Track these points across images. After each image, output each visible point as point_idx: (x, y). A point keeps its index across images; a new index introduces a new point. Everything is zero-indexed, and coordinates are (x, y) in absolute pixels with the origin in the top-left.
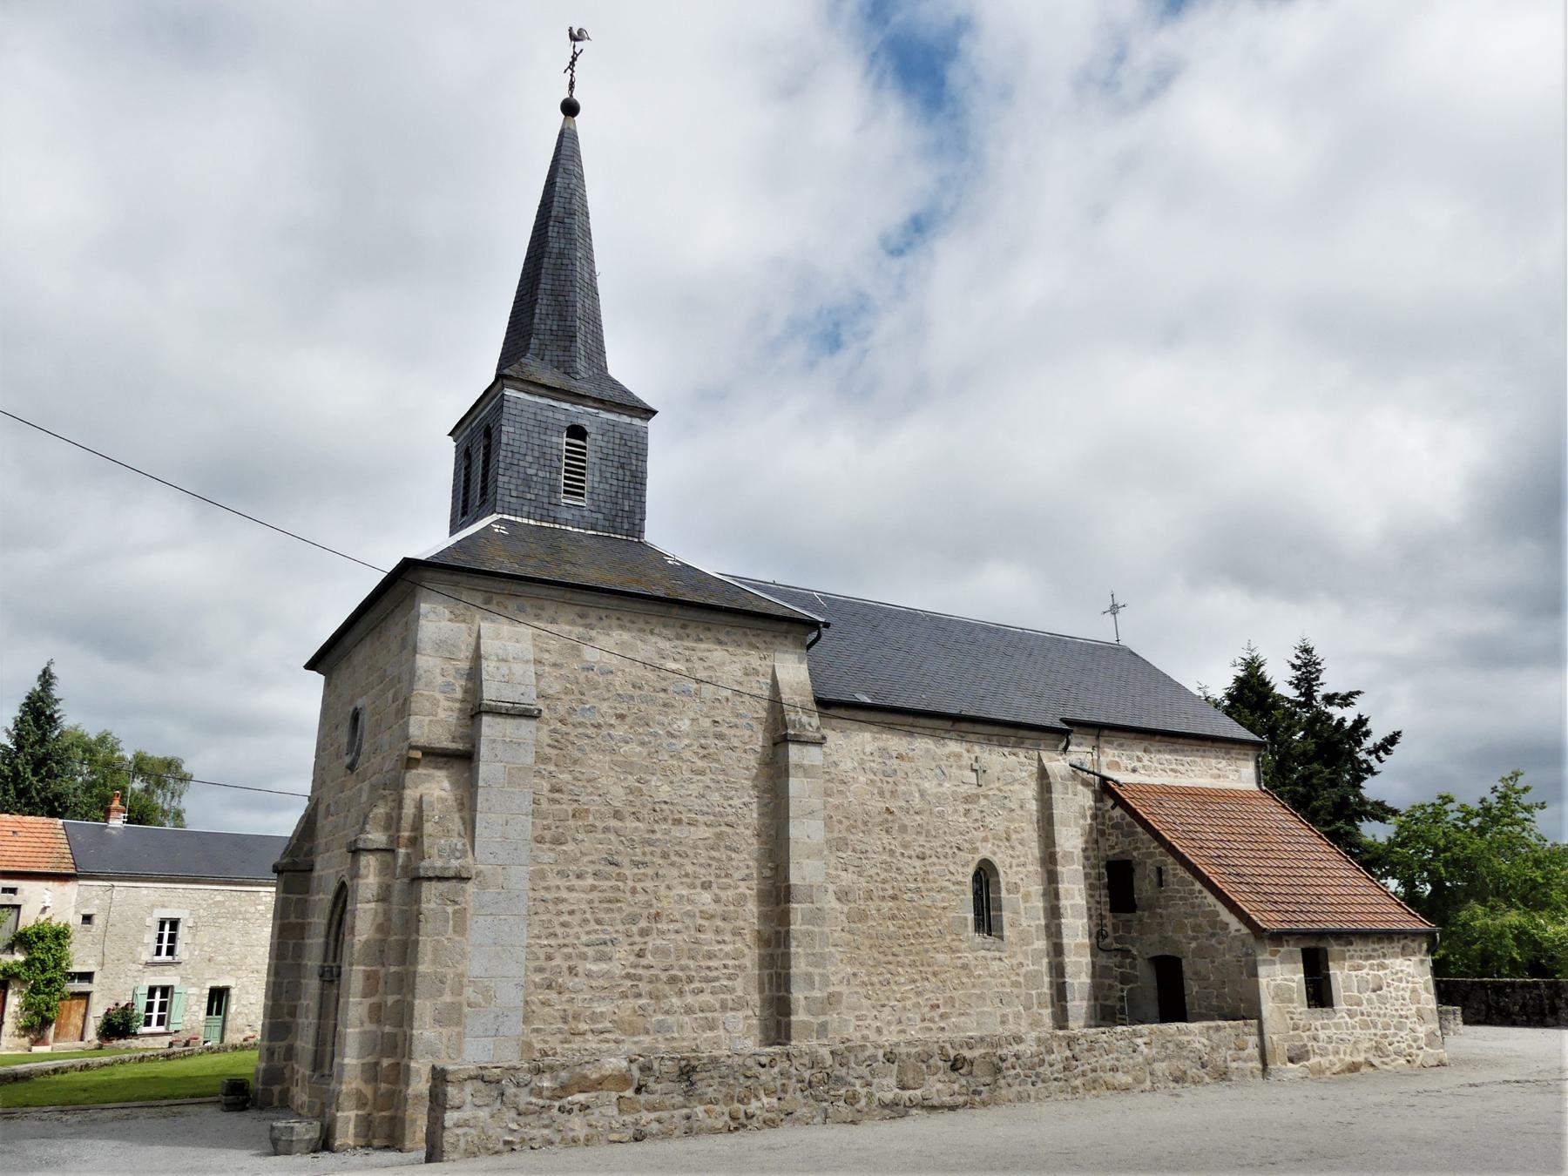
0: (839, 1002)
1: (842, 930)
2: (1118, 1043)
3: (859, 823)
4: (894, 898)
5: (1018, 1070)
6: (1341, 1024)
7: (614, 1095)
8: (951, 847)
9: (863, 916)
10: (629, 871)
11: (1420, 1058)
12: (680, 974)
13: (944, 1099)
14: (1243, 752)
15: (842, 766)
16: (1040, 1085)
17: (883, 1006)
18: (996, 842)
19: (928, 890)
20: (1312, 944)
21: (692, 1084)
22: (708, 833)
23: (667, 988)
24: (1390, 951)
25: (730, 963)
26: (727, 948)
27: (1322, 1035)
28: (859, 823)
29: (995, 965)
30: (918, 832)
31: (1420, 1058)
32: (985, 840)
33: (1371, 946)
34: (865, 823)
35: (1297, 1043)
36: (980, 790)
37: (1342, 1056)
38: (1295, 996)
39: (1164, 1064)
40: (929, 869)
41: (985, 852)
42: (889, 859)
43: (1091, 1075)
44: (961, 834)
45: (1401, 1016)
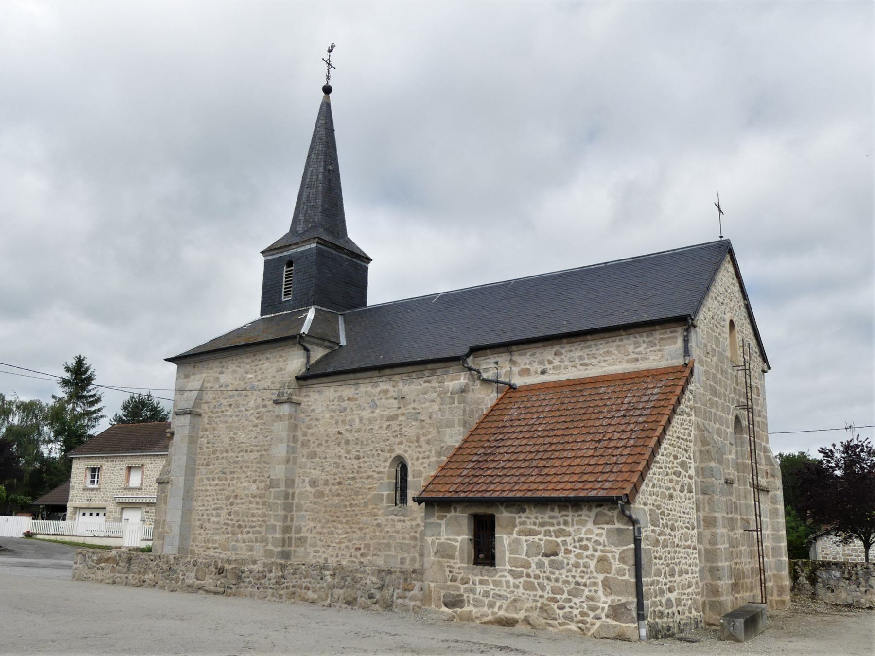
0: (305, 541)
1: (311, 502)
2: (312, 572)
3: (324, 442)
4: (339, 483)
5: (251, 579)
6: (500, 582)
7: (112, 565)
8: (377, 450)
9: (321, 494)
10: (228, 476)
11: (595, 627)
12: (242, 524)
13: (211, 588)
14: (668, 331)
15: (317, 411)
16: (261, 589)
17: (329, 546)
18: (408, 444)
19: (361, 478)
20: (481, 510)
21: (130, 565)
22: (257, 455)
23: (237, 530)
24: (575, 519)
25: (260, 519)
26: (260, 512)
27: (479, 588)
28: (324, 442)
29: (399, 526)
30: (357, 443)
31: (595, 627)
32: (401, 443)
33: (549, 513)
34: (327, 441)
35: (452, 592)
36: (399, 412)
37: (496, 610)
38: (457, 553)
39: (342, 591)
40: (362, 465)
41: (399, 451)
42: (338, 461)
43: (291, 589)
44: (384, 441)
45: (577, 583)
